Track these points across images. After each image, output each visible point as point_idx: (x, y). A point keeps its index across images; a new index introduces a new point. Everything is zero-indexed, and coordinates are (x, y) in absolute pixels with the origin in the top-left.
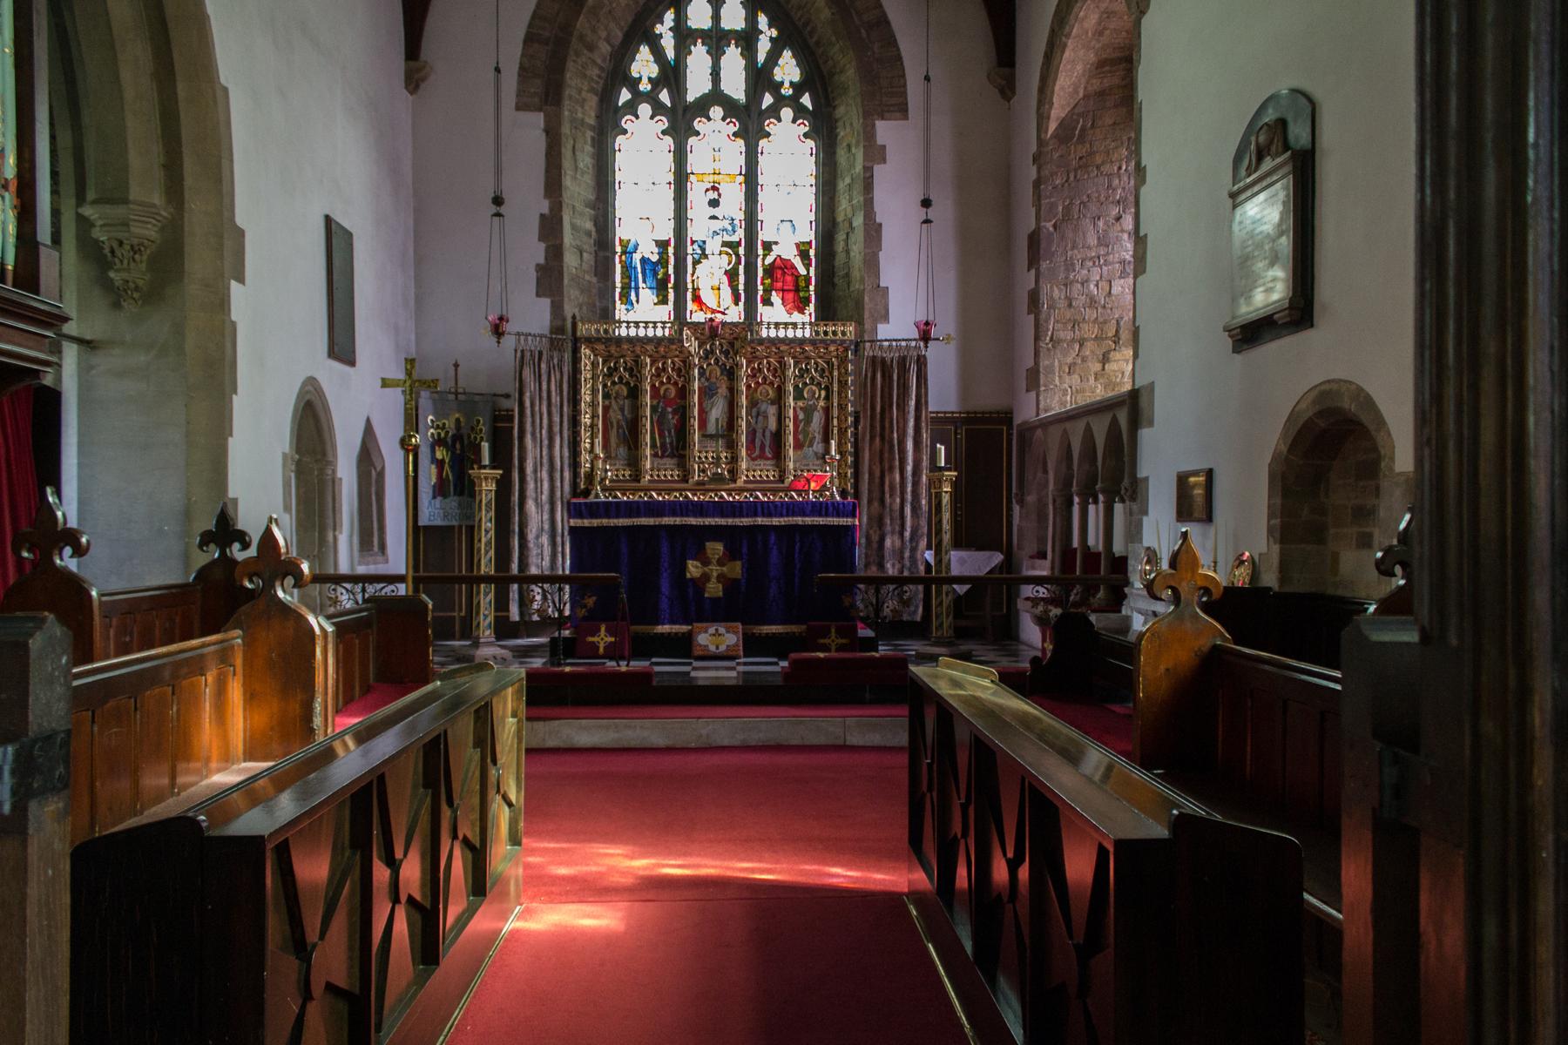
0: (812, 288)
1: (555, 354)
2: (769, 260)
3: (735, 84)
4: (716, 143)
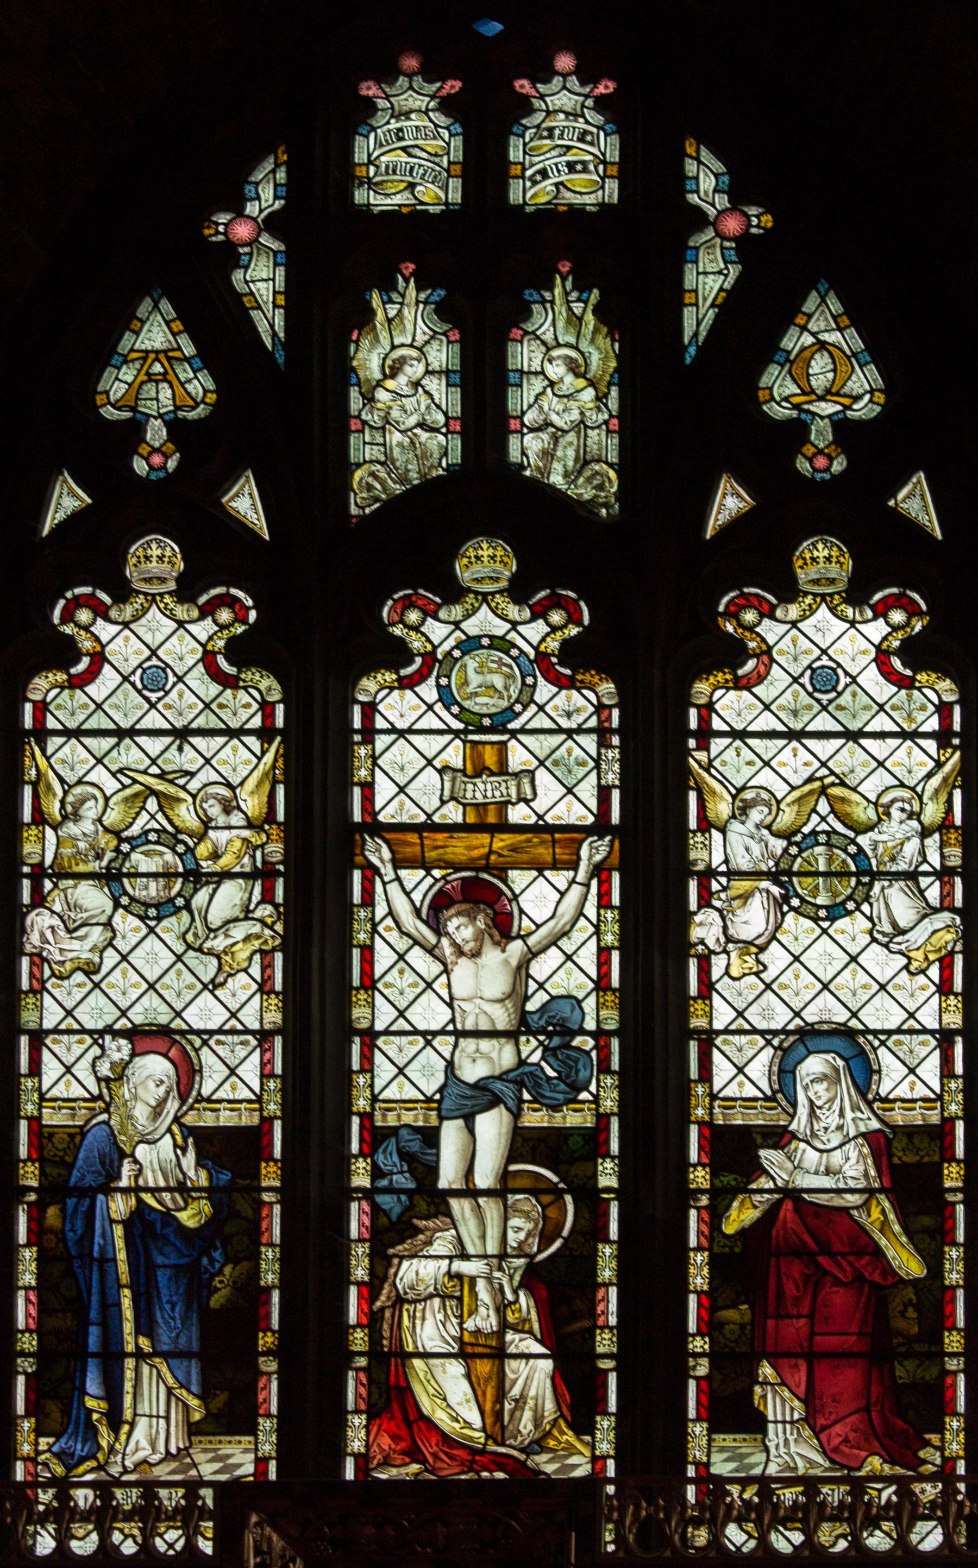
0: (953, 1342)
1: (48, 699)
2: (741, 1216)
3: (565, 397)
4: (475, 717)
